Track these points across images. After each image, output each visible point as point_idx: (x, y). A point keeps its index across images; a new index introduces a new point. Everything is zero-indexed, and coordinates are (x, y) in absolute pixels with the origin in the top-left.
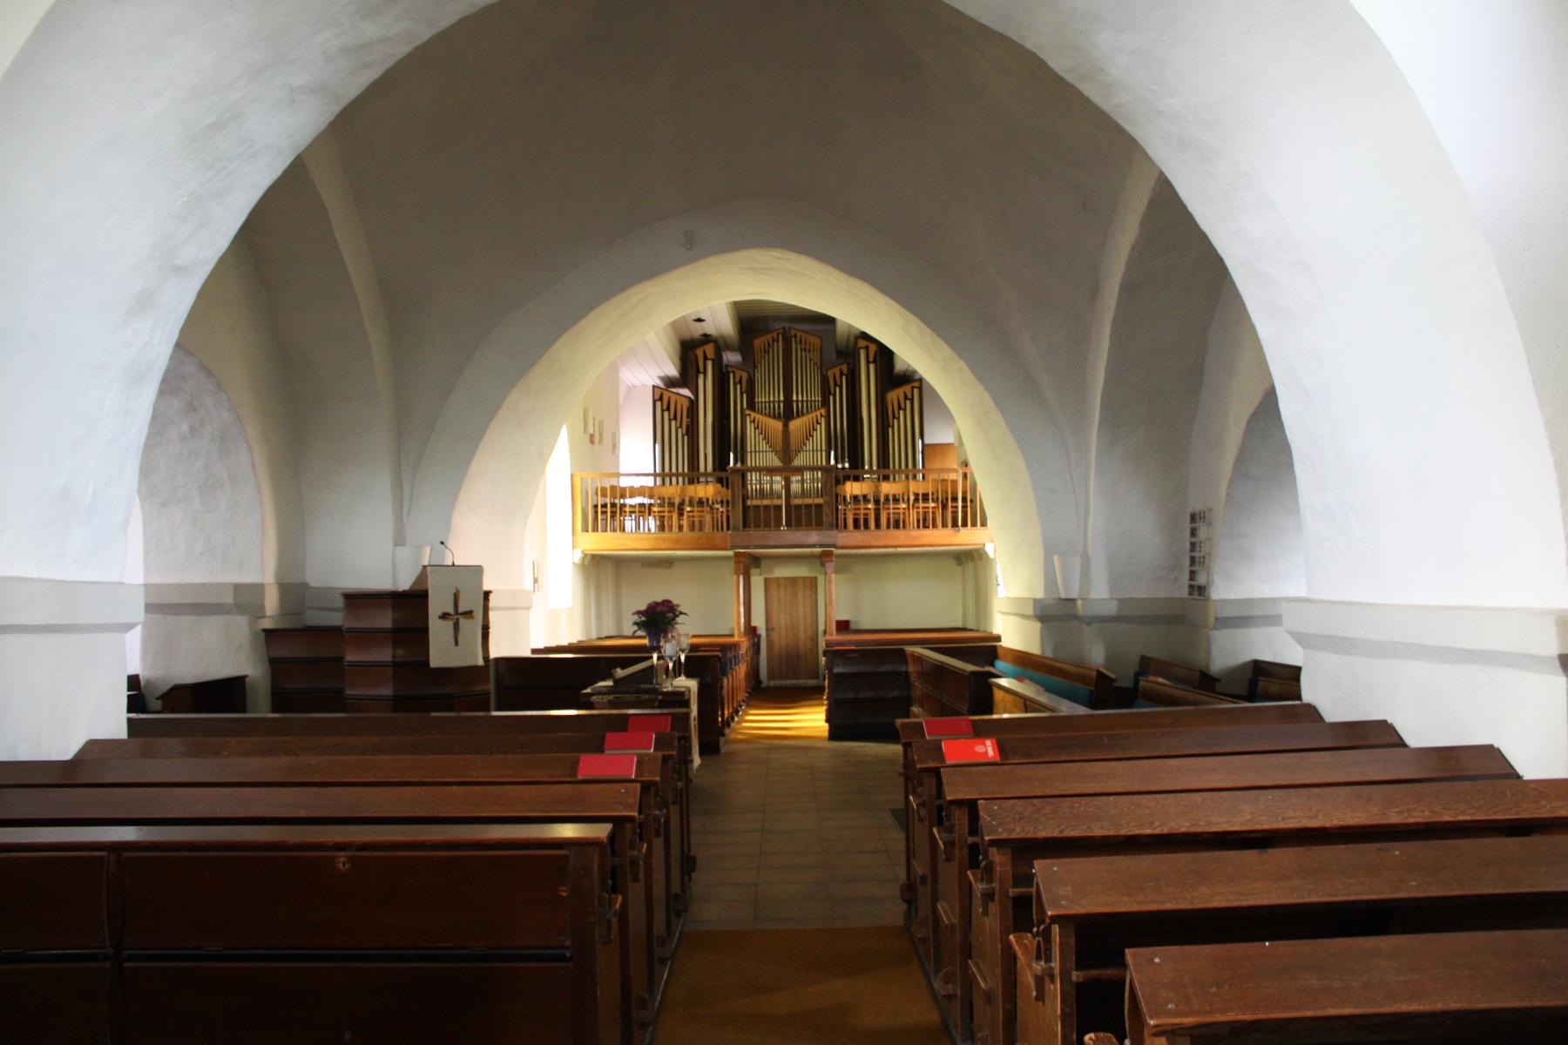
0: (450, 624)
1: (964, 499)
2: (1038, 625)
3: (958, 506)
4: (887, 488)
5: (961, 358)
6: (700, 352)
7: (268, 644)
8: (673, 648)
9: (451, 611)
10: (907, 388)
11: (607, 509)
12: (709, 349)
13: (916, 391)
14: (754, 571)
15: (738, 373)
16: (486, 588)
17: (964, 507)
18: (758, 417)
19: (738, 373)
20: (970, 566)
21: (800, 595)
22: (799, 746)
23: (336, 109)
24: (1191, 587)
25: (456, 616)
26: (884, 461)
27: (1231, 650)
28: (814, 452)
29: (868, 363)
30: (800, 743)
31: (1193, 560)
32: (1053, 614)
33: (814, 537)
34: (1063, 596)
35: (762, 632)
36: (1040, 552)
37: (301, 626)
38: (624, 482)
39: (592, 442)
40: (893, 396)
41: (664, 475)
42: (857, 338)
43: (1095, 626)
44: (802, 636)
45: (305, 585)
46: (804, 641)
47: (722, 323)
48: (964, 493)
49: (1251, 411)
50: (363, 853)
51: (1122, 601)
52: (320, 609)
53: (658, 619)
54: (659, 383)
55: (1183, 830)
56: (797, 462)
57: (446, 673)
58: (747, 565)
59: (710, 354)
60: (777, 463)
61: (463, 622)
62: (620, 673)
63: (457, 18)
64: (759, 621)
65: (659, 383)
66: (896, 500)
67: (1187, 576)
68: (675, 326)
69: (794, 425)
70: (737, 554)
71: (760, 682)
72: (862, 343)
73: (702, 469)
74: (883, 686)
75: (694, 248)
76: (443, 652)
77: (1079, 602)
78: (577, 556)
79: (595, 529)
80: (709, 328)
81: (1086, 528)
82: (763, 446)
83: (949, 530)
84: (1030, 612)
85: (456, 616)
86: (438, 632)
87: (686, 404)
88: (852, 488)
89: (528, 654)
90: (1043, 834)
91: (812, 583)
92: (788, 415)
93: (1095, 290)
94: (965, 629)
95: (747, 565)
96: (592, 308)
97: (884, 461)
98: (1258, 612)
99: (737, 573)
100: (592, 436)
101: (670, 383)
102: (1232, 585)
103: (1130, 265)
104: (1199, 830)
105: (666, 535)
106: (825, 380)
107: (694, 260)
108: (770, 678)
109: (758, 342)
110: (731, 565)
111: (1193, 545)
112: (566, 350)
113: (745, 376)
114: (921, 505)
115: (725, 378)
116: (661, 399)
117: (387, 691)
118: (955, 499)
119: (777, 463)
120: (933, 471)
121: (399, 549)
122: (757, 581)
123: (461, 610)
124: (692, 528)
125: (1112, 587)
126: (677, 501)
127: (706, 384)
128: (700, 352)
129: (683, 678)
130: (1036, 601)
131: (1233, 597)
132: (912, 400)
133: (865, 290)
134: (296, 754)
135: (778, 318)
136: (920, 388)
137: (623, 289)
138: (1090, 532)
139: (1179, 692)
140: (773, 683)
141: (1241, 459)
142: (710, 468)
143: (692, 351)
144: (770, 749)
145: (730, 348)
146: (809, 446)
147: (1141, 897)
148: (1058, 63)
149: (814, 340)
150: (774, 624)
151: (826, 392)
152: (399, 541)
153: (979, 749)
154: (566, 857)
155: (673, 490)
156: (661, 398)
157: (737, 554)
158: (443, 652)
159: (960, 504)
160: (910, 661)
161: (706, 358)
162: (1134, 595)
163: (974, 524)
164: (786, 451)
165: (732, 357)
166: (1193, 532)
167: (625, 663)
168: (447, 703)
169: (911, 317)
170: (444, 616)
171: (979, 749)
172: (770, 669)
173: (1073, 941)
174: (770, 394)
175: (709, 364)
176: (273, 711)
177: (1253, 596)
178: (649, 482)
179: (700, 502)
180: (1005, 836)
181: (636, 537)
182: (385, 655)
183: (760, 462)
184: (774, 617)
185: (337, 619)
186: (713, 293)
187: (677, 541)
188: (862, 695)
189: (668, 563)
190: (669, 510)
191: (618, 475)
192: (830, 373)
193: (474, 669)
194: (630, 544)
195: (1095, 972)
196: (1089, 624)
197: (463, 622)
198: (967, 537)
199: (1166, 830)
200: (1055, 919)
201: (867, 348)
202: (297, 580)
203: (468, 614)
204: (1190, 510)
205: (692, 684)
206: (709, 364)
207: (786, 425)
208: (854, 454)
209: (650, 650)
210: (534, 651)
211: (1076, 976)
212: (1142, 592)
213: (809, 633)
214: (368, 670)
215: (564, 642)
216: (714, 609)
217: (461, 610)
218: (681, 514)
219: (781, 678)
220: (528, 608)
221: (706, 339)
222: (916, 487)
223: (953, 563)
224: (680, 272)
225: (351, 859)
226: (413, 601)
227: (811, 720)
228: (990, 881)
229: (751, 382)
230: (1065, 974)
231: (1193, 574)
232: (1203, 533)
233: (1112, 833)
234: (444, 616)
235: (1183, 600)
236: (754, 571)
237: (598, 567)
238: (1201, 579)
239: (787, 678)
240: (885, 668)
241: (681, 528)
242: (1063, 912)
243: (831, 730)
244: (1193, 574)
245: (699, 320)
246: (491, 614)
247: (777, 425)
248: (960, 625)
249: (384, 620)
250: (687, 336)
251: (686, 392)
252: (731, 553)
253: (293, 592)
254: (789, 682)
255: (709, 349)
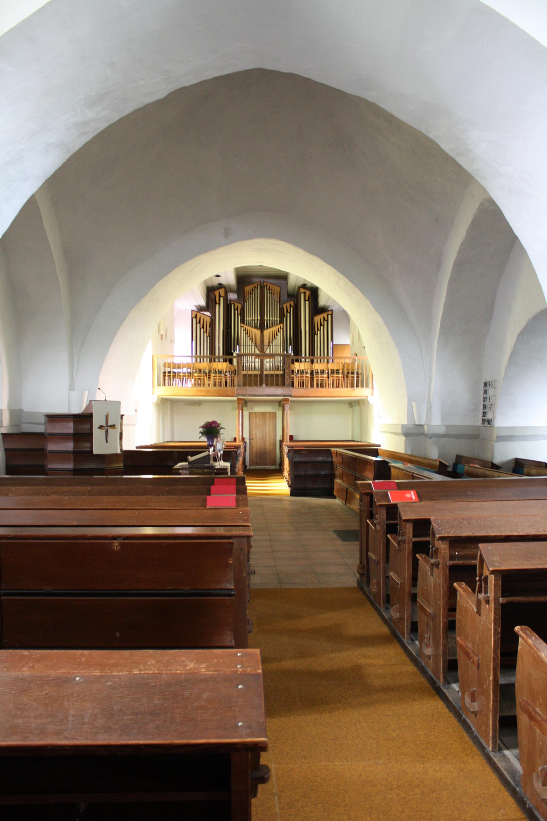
0: (103, 431)
1: (358, 374)
2: (404, 438)
3: (354, 377)
4: (317, 366)
5: (367, 298)
6: (217, 293)
7: (4, 441)
8: (220, 446)
9: (105, 425)
10: (325, 315)
11: (169, 375)
12: (222, 291)
13: (330, 316)
14: (245, 408)
15: (236, 304)
16: (122, 413)
17: (358, 377)
18: (247, 327)
19: (236, 304)
20: (357, 409)
21: (267, 421)
22: (277, 499)
23: (68, 156)
24: (484, 420)
25: (107, 427)
26: (312, 352)
27: (504, 453)
28: (276, 347)
29: (305, 301)
30: (276, 497)
31: (485, 407)
32: (413, 433)
33: (279, 391)
34: (417, 423)
35: (247, 440)
36: (405, 400)
37: (19, 432)
38: (177, 361)
39: (162, 339)
40: (318, 319)
41: (198, 357)
42: (299, 288)
43: (433, 439)
44: (268, 443)
45: (21, 411)
46: (269, 447)
47: (230, 279)
48: (358, 369)
49: (520, 330)
50: (126, 541)
51: (447, 426)
52: (29, 423)
53: (211, 430)
54: (195, 309)
55: (532, 533)
56: (267, 352)
57: (102, 457)
58: (243, 404)
59: (222, 294)
60: (257, 352)
61: (110, 430)
62: (191, 459)
63: (133, 109)
64: (246, 436)
65: (195, 309)
66: (323, 372)
67: (481, 414)
68: (205, 282)
69: (266, 332)
70: (239, 399)
71: (246, 467)
72: (302, 290)
73: (217, 354)
74: (316, 470)
75: (229, 237)
76: (100, 447)
77: (426, 427)
78: (155, 399)
79: (164, 385)
80: (222, 280)
81: (430, 389)
82: (250, 343)
83: (350, 389)
84: (399, 430)
85: (107, 427)
86: (98, 435)
87: (209, 320)
88: (297, 366)
89: (134, 449)
90: (465, 534)
91: (274, 415)
92: (262, 327)
93: (439, 266)
94: (354, 441)
95: (243, 404)
96: (175, 267)
97: (312, 352)
98: (518, 434)
99: (238, 409)
100: (162, 335)
101: (201, 309)
102: (504, 420)
103: (460, 252)
104: (541, 533)
105: (202, 388)
106: (282, 310)
107: (230, 243)
108: (251, 464)
109: (247, 289)
110: (236, 404)
111: (485, 399)
112: (160, 288)
113: (240, 306)
114: (335, 375)
115: (232, 306)
116: (196, 317)
117: (70, 466)
118: (353, 373)
119: (257, 352)
120: (339, 358)
121: (72, 392)
122: (246, 414)
123: (109, 424)
124: (215, 385)
125: (443, 420)
126: (207, 371)
127: (220, 310)
128: (217, 293)
129: (222, 461)
130: (403, 426)
131: (506, 426)
132: (327, 321)
133: (317, 262)
134: (48, 495)
135: (257, 276)
136: (332, 315)
137: (191, 258)
138: (432, 390)
139: (481, 471)
140: (252, 467)
141: (513, 354)
142: (221, 354)
143: (212, 292)
144: (261, 500)
145: (232, 291)
146: (274, 343)
147: (533, 562)
148: (446, 146)
149: (277, 289)
150: (254, 437)
151: (282, 316)
152: (72, 388)
153: (408, 495)
154: (232, 543)
155: (205, 365)
156: (195, 317)
157: (239, 399)
158: (100, 447)
159: (355, 375)
160: (334, 456)
161: (220, 296)
162: (453, 424)
163: (362, 386)
164: (262, 347)
165: (233, 296)
166: (485, 392)
167: (193, 454)
168: (101, 472)
169: (342, 276)
170: (101, 427)
171: (408, 495)
172: (251, 459)
173: (500, 583)
174: (253, 316)
175: (222, 299)
176: (7, 474)
177: (515, 426)
178: (189, 360)
179: (220, 372)
180: (446, 535)
181: (184, 390)
182: (69, 446)
183: (248, 352)
184: (254, 433)
185: (41, 429)
186: (224, 264)
187: (208, 392)
188: (308, 473)
189: (198, 403)
190: (201, 376)
191: (173, 356)
192: (285, 306)
193: (116, 455)
194: (183, 393)
195: (511, 599)
196: (430, 438)
197: (110, 430)
198: (359, 393)
199: (524, 533)
200: (493, 572)
201: (305, 293)
202: (18, 408)
203: (113, 426)
204: (484, 380)
205: (228, 465)
206: (222, 299)
207: (262, 332)
208: (297, 351)
209: (207, 447)
210: (137, 448)
211: (501, 600)
212: (458, 422)
213: (272, 441)
214: (61, 455)
215: (148, 444)
216: (235, 428)
217: (109, 424)
218: (209, 378)
219: (257, 465)
220: (135, 425)
221: (220, 286)
222: (331, 366)
223: (348, 406)
224: (222, 249)
225: (121, 544)
226: (85, 418)
227: (280, 486)
228: (437, 558)
229: (243, 309)
230: (496, 599)
231: (484, 414)
232: (491, 392)
233: (498, 534)
234: (101, 427)
235: (478, 427)
236: (245, 408)
237: (167, 405)
238: (489, 416)
239: (260, 465)
240: (320, 459)
241: (209, 385)
242: (496, 568)
243: (291, 492)
244: (484, 414)
245: (218, 276)
246: (124, 427)
247: (258, 332)
248: (350, 439)
249: (69, 428)
250: (210, 284)
251: (208, 314)
252: (235, 398)
253: (16, 414)
254: (260, 467)
255: (222, 291)
